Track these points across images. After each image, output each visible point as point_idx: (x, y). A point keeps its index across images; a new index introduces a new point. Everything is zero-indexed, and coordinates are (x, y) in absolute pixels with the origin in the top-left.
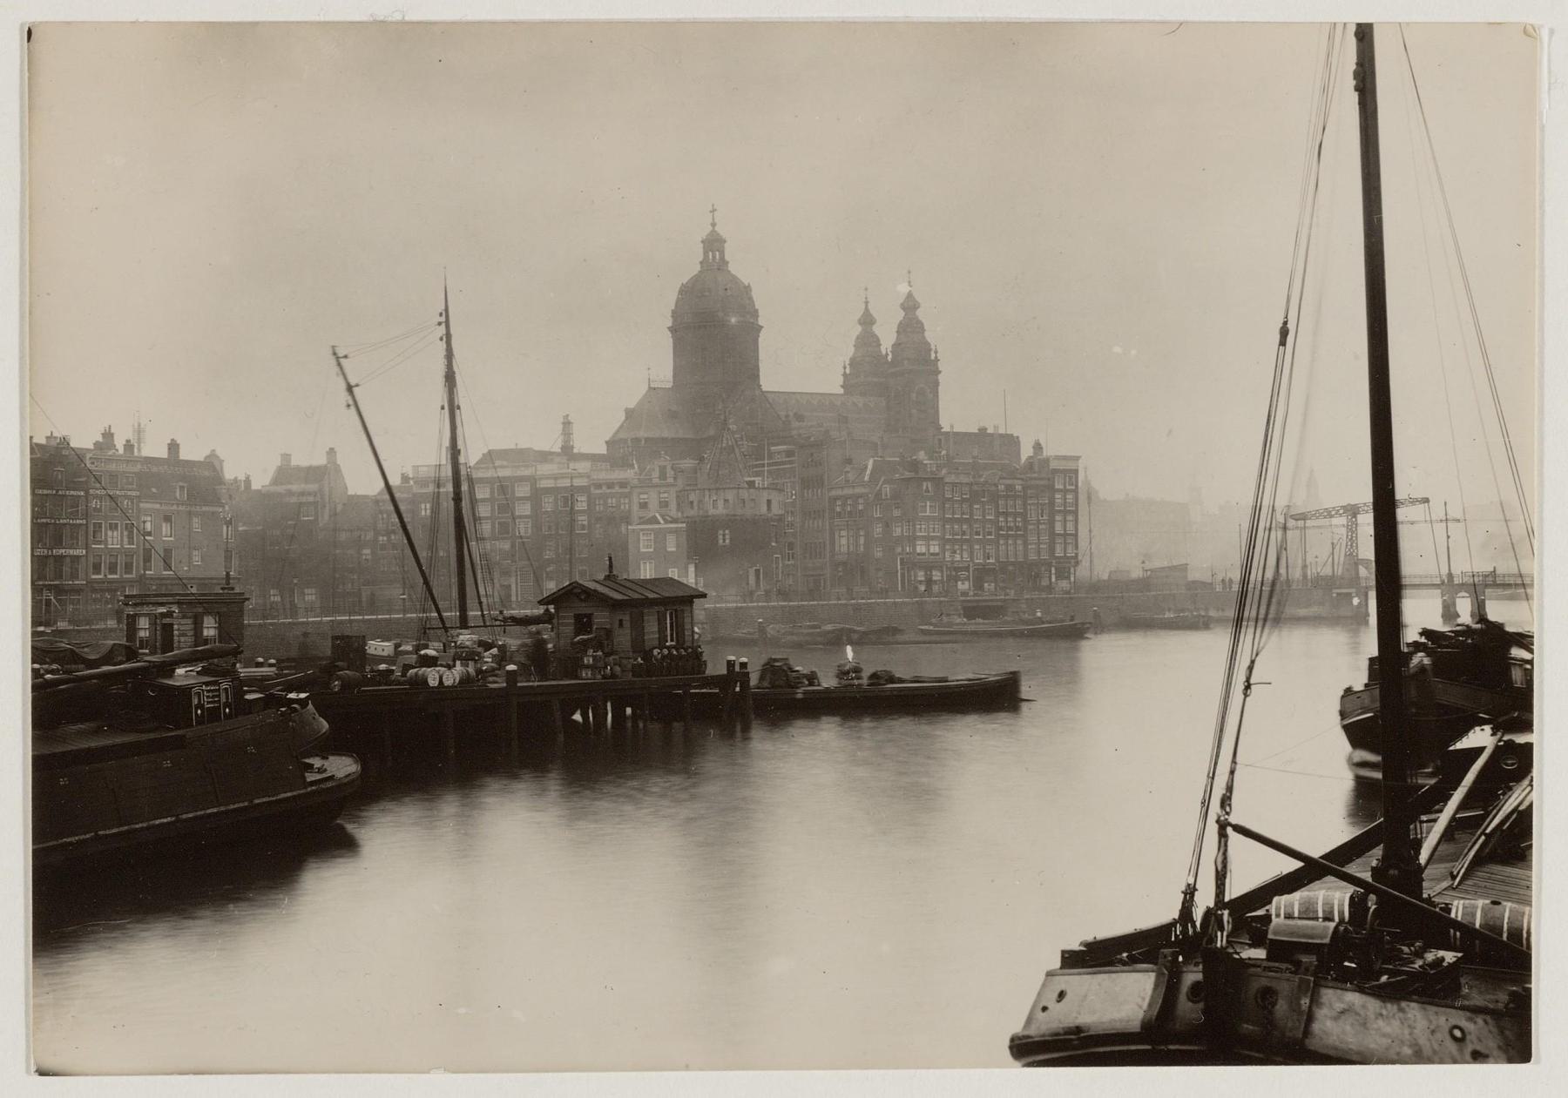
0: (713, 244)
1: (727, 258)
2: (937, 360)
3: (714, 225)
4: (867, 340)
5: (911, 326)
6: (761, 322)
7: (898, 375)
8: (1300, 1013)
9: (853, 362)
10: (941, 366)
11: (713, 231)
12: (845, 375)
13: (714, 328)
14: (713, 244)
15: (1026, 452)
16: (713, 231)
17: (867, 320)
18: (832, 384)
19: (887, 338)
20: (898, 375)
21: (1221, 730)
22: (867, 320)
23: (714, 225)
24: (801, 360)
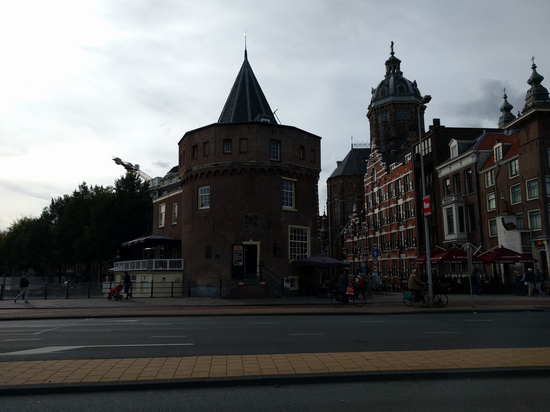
0: (393, 64)
3: (393, 53)
11: (393, 56)
14: (393, 64)
16: (393, 56)
17: (507, 108)
23: (393, 53)
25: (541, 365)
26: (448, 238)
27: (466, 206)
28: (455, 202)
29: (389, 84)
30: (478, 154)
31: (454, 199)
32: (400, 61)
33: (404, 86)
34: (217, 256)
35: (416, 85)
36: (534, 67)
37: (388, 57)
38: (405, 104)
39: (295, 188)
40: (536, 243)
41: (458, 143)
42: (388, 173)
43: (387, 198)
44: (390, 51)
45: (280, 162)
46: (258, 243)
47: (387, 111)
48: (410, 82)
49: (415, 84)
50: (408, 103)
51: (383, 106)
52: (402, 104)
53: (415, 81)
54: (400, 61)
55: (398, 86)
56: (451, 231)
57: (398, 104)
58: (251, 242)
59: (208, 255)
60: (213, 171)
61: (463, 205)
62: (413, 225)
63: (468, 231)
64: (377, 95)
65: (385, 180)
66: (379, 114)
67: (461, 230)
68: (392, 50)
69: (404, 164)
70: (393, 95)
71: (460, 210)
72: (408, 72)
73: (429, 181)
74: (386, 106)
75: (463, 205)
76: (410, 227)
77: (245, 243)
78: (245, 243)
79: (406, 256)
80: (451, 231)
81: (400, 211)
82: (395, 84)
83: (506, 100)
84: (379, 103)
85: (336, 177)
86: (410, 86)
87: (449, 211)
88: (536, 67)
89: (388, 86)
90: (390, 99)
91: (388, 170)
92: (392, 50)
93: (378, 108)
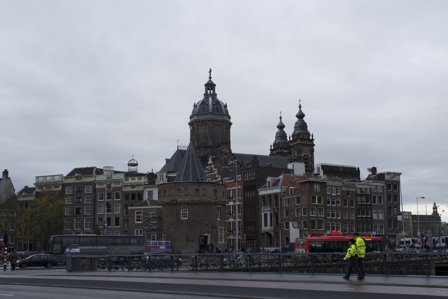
0: (210, 86)
1: (216, 92)
2: (313, 139)
3: (210, 78)
4: (281, 135)
5: (301, 125)
6: (231, 121)
7: (296, 143)
8: (279, 263)
9: (274, 144)
10: (315, 142)
11: (210, 80)
12: (271, 150)
13: (211, 120)
14: (210, 86)
15: (364, 174)
16: (210, 80)
17: (281, 127)
18: (267, 152)
19: (289, 131)
20: (296, 143)
21: (205, 279)
22: (281, 127)
23: (210, 78)
24: (251, 138)
26: (264, 229)
27: (274, 213)
28: (269, 211)
29: (208, 103)
30: (281, 188)
31: (268, 209)
32: (215, 85)
33: (219, 107)
34: (192, 240)
35: (227, 106)
36: (300, 107)
37: (206, 80)
38: (219, 121)
40: (305, 234)
44: (209, 76)
45: (217, 199)
46: (209, 235)
47: (206, 125)
49: (226, 106)
51: (204, 121)
52: (217, 121)
53: (226, 105)
54: (215, 85)
55: (215, 106)
56: (266, 225)
58: (207, 235)
59: (188, 240)
61: (272, 212)
63: (274, 226)
64: (199, 111)
66: (200, 125)
67: (271, 225)
68: (210, 75)
69: (235, 181)
70: (211, 113)
71: (271, 214)
72: (221, 97)
73: (252, 195)
75: (272, 212)
78: (204, 235)
80: (266, 225)
82: (213, 105)
83: (281, 120)
84: (201, 118)
86: (223, 108)
87: (266, 215)
89: (208, 105)
90: (210, 117)
92: (210, 75)
93: (199, 121)
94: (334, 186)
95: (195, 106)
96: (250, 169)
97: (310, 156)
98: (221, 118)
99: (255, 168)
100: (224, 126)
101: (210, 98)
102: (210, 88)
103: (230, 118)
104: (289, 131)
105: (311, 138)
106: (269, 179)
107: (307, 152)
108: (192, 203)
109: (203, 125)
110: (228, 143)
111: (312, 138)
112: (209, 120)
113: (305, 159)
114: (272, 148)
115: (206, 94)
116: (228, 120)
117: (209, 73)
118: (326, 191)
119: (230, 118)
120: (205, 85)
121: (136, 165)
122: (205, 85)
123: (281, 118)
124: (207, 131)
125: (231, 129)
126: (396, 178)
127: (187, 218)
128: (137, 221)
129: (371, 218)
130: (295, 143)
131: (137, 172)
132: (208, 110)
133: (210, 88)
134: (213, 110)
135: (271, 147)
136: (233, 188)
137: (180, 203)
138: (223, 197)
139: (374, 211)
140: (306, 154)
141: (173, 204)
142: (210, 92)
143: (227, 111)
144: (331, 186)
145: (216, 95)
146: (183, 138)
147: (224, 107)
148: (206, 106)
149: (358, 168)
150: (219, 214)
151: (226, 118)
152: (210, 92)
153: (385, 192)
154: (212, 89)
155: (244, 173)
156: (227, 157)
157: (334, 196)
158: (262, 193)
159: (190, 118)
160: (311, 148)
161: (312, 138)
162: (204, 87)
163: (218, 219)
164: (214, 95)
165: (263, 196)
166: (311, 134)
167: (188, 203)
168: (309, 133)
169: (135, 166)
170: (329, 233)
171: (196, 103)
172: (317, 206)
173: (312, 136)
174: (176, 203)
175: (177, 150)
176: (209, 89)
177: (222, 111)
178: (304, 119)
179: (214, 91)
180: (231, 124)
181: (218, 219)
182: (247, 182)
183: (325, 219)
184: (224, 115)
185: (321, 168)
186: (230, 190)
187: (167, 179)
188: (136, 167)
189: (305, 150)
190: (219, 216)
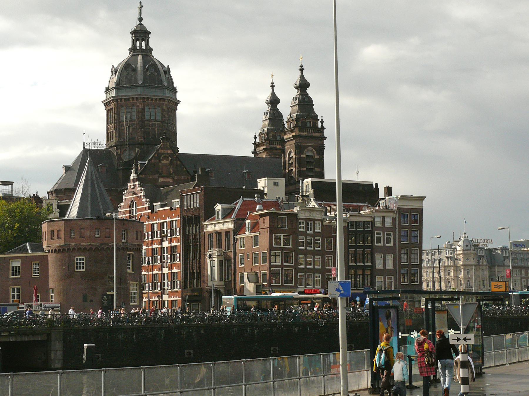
1: (151, 45)
2: (323, 128)
3: (141, 19)
4: (275, 116)
6: (179, 97)
12: (255, 144)
17: (274, 101)
19: (287, 109)
22: (274, 101)
23: (141, 19)
25: (154, 90)
27: (225, 260)
29: (136, 67)
34: (91, 301)
35: (169, 71)
37: (133, 25)
38: (156, 99)
39: (133, 258)
41: (222, 208)
42: (152, 212)
43: (150, 237)
44: (137, 16)
47: (133, 105)
48: (163, 66)
49: (167, 71)
50: (160, 99)
52: (152, 99)
54: (150, 33)
55: (148, 73)
57: (148, 99)
59: (85, 300)
60: (94, 248)
62: (179, 269)
65: (149, 218)
68: (140, 14)
69: (171, 209)
70: (142, 86)
72: (161, 54)
74: (133, 98)
75: (222, 259)
76: (174, 270)
77: (108, 293)
78: (108, 293)
79: (169, 298)
81: (164, 253)
82: (145, 70)
84: (124, 94)
85: (66, 189)
86: (163, 74)
88: (303, 69)
89: (135, 70)
90: (138, 92)
91: (151, 207)
92: (140, 14)
93: (121, 99)
94: (310, 219)
95: (114, 71)
96: (193, 190)
97: (317, 157)
98: (157, 94)
99: (220, 180)
100: (165, 108)
101: (140, 58)
102: (140, 38)
103: (176, 92)
104: (287, 109)
105: (320, 125)
106: (218, 207)
107: (311, 151)
108: (91, 249)
109: (127, 106)
110: (171, 137)
111: (322, 126)
112: (137, 98)
113: (308, 163)
114: (257, 140)
115: (133, 49)
116: (174, 98)
117: (138, 11)
118: (297, 228)
119: (174, 91)
120: (132, 33)
121: (11, 183)
122: (132, 33)
123: (273, 86)
124: (134, 117)
125: (177, 111)
126: (413, 205)
127: (84, 270)
128: (13, 275)
129: (373, 267)
130: (291, 136)
131: (12, 195)
132: (136, 79)
133: (140, 38)
134: (145, 80)
135: (255, 138)
136: (167, 220)
137: (74, 249)
138: (137, 239)
139: (413, 252)
140: (310, 154)
141: (64, 250)
142: (141, 44)
143: (170, 81)
144: (306, 220)
145: (151, 50)
146: (95, 129)
147: (165, 72)
148: (132, 73)
149: (377, 185)
150: (131, 264)
151: (168, 94)
152: (141, 44)
153: (397, 227)
154: (143, 40)
155: (183, 197)
156: (168, 162)
157: (310, 235)
158: (210, 228)
159: (106, 92)
160: (320, 142)
161: (322, 126)
162: (130, 35)
163: (129, 271)
164: (148, 52)
165: (210, 235)
166: (320, 118)
167: (85, 249)
168: (317, 116)
169: (8, 185)
170: (302, 290)
171: (115, 67)
172: (282, 249)
173: (322, 122)
174: (68, 249)
175: (82, 149)
176: (138, 40)
177: (161, 82)
178: (279, 106)
179: (147, 44)
180: (177, 103)
181: (129, 271)
182: (188, 210)
183: (295, 269)
184: (164, 87)
185: (310, 187)
186: (163, 223)
187: (58, 210)
188: (10, 186)
189: (307, 147)
190: (131, 267)
